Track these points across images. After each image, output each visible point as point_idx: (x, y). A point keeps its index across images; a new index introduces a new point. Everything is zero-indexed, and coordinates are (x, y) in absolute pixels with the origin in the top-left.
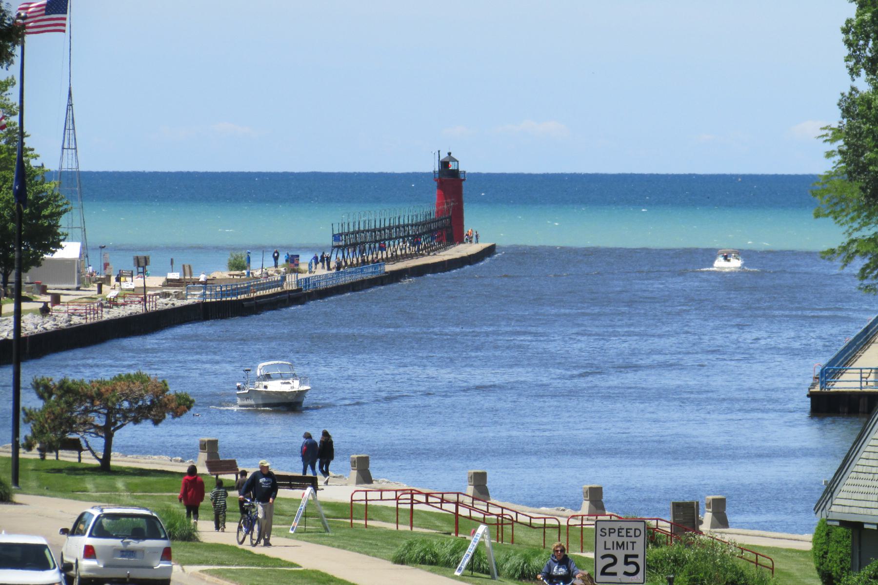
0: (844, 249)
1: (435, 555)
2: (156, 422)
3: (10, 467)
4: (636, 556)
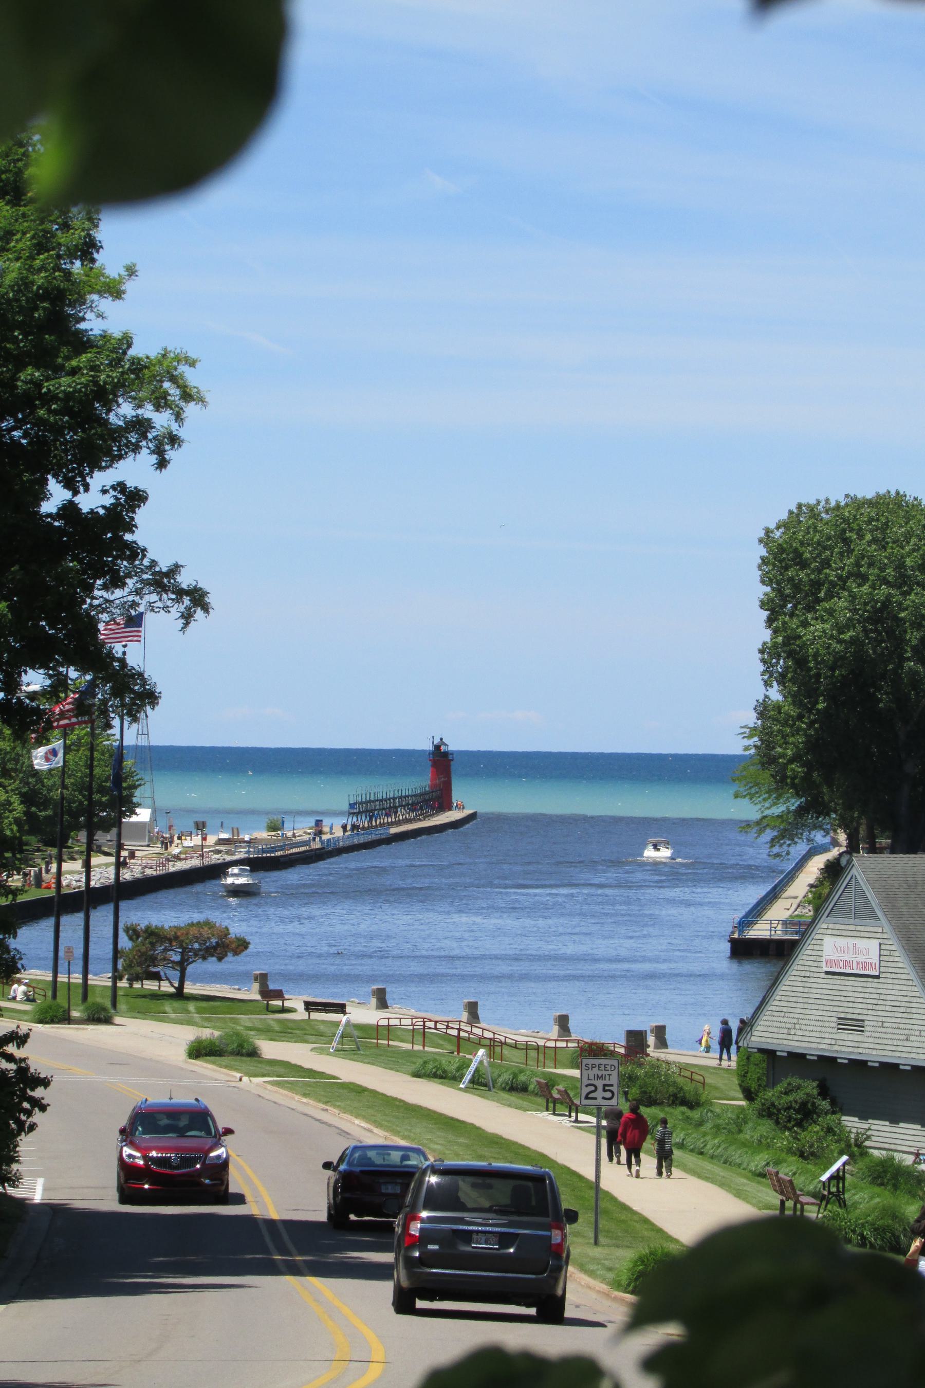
0: (758, 823)
1: (445, 1071)
2: (220, 959)
3: (109, 993)
4: (612, 1085)
